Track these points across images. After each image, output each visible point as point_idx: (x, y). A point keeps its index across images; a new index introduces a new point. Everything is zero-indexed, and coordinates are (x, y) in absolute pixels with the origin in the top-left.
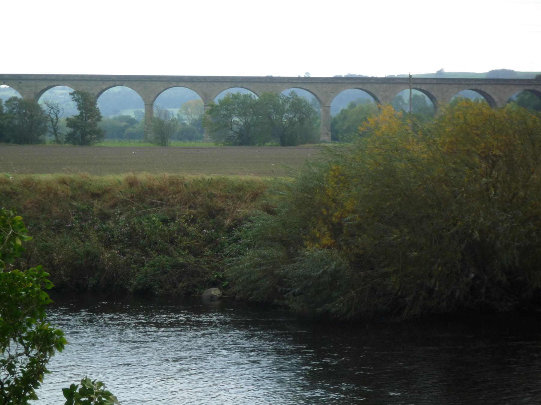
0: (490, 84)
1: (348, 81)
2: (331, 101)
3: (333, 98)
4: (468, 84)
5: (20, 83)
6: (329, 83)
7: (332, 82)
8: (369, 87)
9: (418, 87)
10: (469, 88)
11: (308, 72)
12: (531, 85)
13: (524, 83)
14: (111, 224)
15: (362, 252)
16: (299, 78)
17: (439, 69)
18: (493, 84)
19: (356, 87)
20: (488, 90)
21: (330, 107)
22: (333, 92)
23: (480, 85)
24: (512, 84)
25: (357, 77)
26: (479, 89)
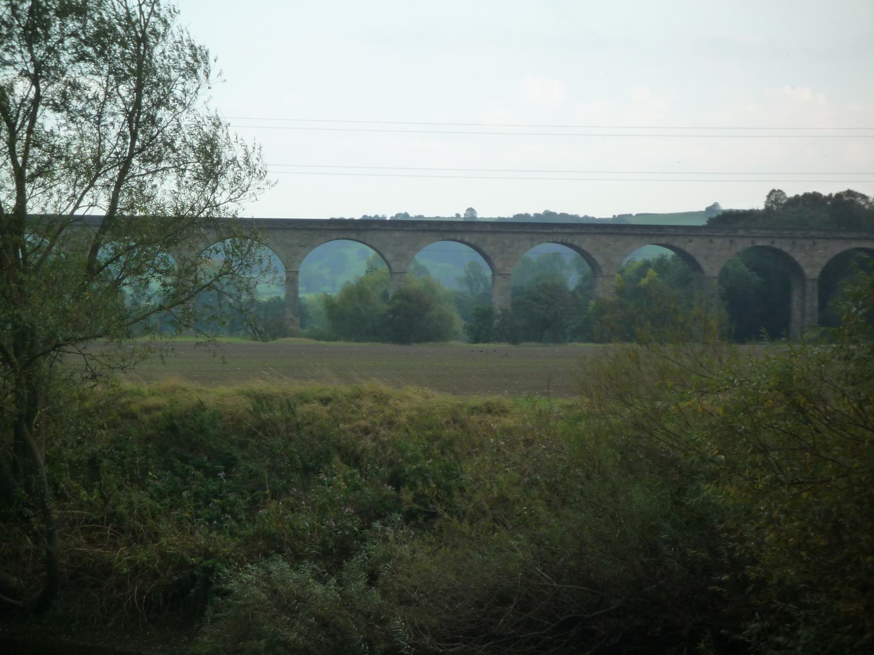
0: (589, 234)
1: (332, 227)
2: (300, 262)
3: (304, 257)
4: (549, 234)
5: (711, 242)
6: (295, 229)
7: (300, 227)
8: (587, 243)
9: (459, 238)
10: (551, 241)
11: (474, 208)
12: (663, 235)
13: (652, 233)
14: (407, 488)
15: (203, 542)
16: (352, 222)
17: (710, 204)
18: (595, 233)
19: (659, 242)
20: (691, 247)
21: (298, 272)
22: (304, 246)
23: (570, 234)
24: (628, 234)
25: (506, 221)
26: (569, 241)
